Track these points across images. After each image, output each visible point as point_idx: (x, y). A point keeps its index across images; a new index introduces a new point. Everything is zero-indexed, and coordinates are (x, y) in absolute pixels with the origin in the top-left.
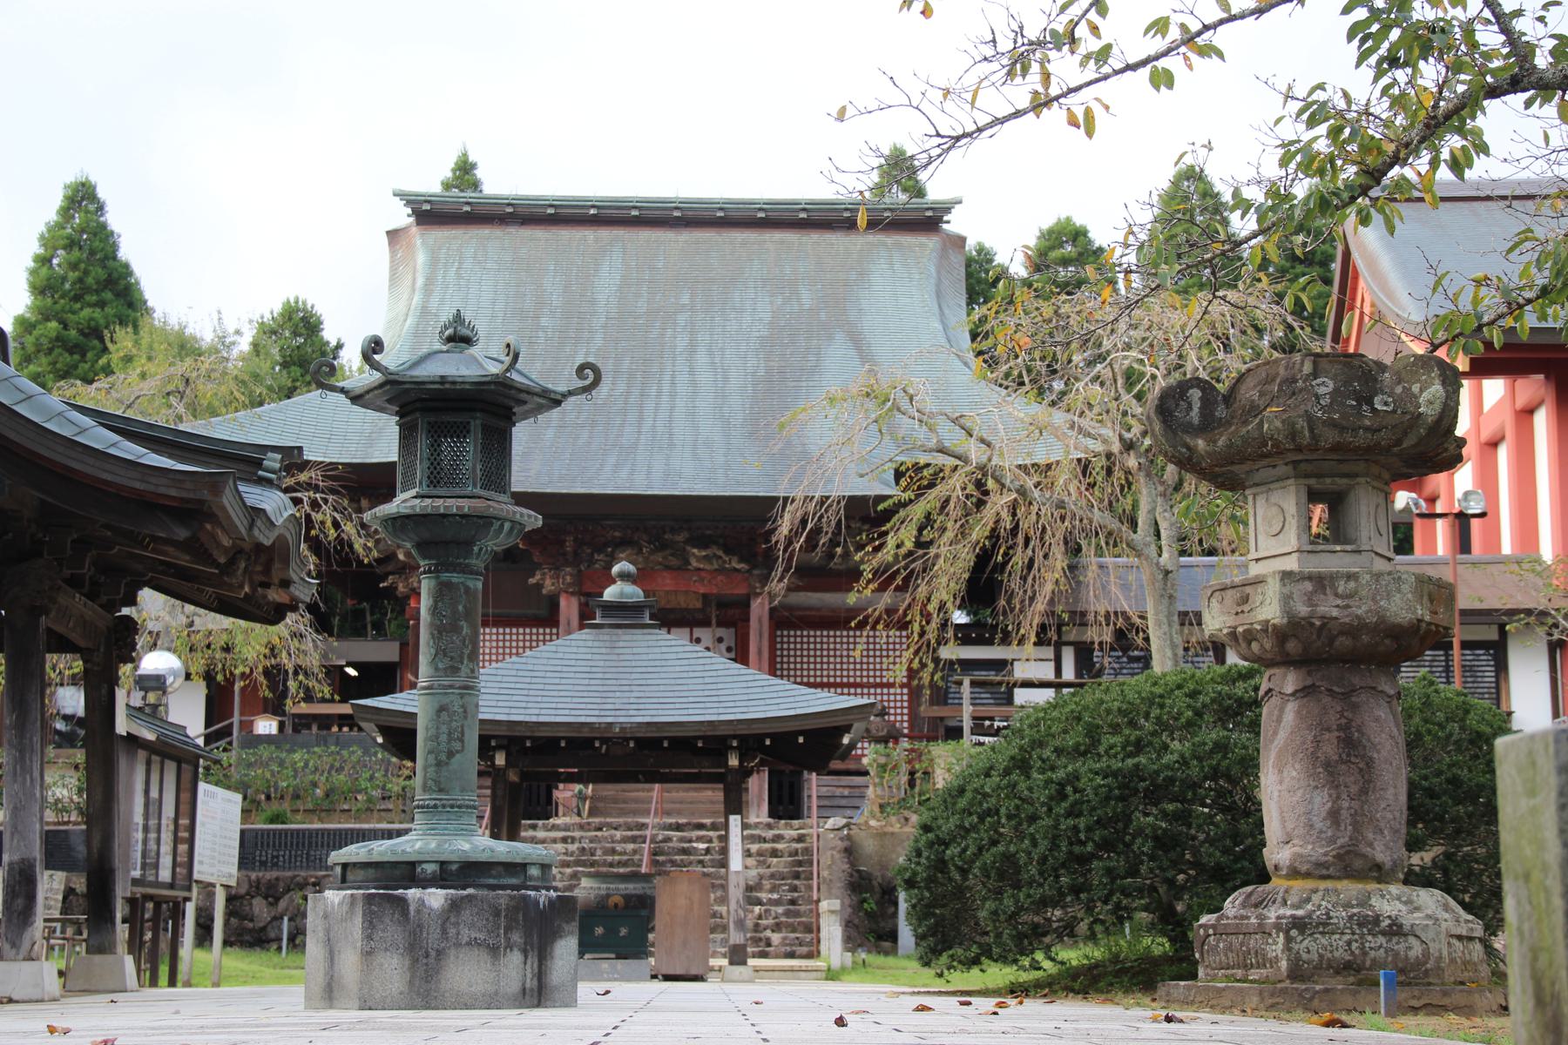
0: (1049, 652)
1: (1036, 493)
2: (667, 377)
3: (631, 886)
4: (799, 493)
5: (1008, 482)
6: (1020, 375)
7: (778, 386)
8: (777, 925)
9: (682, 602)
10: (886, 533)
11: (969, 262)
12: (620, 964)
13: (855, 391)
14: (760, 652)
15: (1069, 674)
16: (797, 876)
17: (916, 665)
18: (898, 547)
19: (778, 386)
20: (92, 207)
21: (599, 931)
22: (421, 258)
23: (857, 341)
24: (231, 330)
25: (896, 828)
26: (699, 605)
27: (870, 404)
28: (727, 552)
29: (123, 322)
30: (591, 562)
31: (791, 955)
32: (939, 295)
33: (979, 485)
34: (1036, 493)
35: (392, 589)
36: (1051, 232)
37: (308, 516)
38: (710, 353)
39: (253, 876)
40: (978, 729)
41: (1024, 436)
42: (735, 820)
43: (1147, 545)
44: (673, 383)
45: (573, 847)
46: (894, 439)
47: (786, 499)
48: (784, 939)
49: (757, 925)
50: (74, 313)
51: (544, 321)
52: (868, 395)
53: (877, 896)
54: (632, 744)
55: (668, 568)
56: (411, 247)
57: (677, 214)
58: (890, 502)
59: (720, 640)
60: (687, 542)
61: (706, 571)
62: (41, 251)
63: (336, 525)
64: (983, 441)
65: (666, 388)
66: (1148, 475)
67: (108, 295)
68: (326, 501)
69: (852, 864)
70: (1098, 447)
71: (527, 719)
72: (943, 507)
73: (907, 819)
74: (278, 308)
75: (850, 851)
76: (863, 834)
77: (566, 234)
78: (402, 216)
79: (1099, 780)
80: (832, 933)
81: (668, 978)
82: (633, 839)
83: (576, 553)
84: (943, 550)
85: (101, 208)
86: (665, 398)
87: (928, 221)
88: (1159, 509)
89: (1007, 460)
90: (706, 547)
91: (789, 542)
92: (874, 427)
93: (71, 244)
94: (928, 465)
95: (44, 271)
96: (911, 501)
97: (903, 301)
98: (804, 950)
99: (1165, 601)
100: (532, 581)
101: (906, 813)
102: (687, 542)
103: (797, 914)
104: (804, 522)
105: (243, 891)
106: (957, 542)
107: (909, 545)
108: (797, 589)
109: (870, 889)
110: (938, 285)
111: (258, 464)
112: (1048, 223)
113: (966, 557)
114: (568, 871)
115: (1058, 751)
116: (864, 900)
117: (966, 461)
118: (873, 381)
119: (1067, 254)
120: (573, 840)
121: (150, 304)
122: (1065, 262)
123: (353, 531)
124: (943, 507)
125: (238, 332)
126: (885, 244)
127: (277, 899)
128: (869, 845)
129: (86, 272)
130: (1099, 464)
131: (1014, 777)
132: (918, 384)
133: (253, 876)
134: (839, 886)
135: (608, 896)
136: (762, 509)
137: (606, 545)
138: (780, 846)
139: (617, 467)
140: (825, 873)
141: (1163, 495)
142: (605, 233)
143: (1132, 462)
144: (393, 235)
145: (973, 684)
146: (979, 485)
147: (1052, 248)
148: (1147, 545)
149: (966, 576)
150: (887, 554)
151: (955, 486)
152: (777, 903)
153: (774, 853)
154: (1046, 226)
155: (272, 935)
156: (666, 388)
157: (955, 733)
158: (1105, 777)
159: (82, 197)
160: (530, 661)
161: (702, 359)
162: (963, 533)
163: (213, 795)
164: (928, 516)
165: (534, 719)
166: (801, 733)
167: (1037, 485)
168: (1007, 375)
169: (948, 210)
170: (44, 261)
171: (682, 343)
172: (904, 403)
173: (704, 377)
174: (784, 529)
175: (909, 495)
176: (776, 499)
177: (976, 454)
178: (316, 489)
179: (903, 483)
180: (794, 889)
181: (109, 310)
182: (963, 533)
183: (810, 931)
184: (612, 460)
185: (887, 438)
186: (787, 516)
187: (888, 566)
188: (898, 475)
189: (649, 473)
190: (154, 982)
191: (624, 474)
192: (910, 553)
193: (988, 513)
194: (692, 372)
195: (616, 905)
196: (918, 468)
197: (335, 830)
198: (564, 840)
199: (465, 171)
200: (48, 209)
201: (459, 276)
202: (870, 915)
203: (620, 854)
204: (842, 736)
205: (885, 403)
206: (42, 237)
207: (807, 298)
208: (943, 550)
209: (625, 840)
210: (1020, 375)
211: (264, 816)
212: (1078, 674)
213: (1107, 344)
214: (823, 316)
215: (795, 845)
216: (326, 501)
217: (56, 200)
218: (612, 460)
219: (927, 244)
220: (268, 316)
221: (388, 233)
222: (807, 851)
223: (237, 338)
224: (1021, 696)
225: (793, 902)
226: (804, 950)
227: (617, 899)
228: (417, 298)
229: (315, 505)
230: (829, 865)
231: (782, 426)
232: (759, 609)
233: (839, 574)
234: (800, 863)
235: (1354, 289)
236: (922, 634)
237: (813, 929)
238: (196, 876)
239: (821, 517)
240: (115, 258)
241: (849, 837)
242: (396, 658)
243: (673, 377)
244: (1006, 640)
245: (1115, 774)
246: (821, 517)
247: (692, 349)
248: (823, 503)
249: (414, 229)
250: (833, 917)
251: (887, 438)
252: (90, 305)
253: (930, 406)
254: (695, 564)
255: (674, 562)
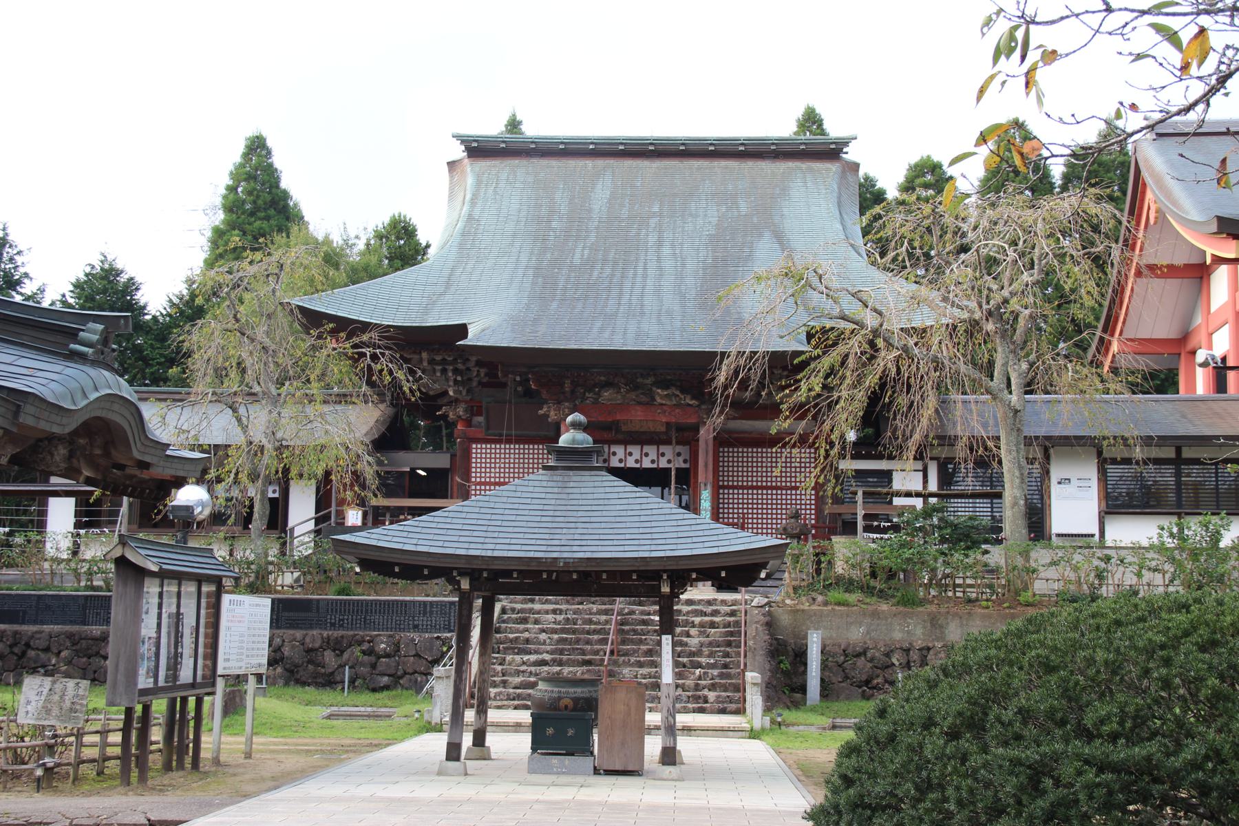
0: (919, 465)
1: (916, 351)
2: (641, 264)
3: (579, 690)
4: (733, 350)
5: (896, 344)
6: (903, 261)
7: (723, 269)
8: (713, 685)
9: (651, 427)
10: (800, 380)
11: (861, 185)
12: (567, 760)
13: (777, 272)
14: (706, 465)
15: (933, 486)
16: (729, 644)
17: (821, 480)
18: (810, 390)
19: (723, 269)
20: (264, 153)
21: (550, 731)
22: (470, 180)
23: (780, 238)
24: (353, 236)
25: (806, 606)
26: (663, 429)
27: (787, 282)
28: (682, 392)
29: (280, 230)
30: (584, 399)
31: (723, 711)
32: (839, 205)
33: (872, 344)
34: (916, 351)
35: (445, 417)
36: (916, 166)
37: (369, 366)
38: (673, 246)
39: (325, 634)
40: (868, 529)
41: (904, 305)
42: (667, 640)
43: (1001, 390)
44: (645, 269)
45: (560, 618)
46: (807, 309)
47: (723, 354)
48: (718, 697)
49: (697, 685)
50: (250, 224)
51: (554, 224)
52: (787, 274)
53: (791, 658)
54: (575, 577)
55: (640, 403)
56: (463, 172)
57: (651, 148)
58: (803, 357)
59: (679, 454)
60: (654, 384)
61: (667, 406)
62: (231, 183)
63: (391, 373)
64: (875, 310)
65: (640, 271)
66: (1003, 337)
67: (272, 212)
68: (383, 355)
69: (772, 635)
70: (966, 315)
71: (484, 553)
72: (843, 363)
73: (814, 599)
74: (387, 221)
75: (771, 625)
76: (780, 610)
77: (572, 163)
78: (458, 151)
79: (1090, 775)
80: (755, 700)
81: (609, 773)
82: (606, 612)
83: (573, 392)
84: (844, 394)
85: (269, 153)
86: (639, 279)
87: (831, 152)
88: (1011, 363)
89: (894, 324)
90: (667, 388)
91: (726, 387)
92: (791, 300)
93: (250, 177)
94: (832, 328)
95: (231, 196)
96: (819, 357)
97: (814, 215)
98: (733, 706)
99: (1015, 433)
100: (541, 412)
101: (814, 594)
102: (654, 384)
103: (728, 676)
104: (736, 373)
105: (317, 645)
106: (855, 387)
107: (818, 389)
108: (734, 418)
109: (785, 653)
110: (839, 197)
111: (73, 335)
112: (914, 159)
113: (861, 395)
114: (556, 636)
115: (1025, 714)
116: (781, 662)
117: (862, 325)
118: (790, 264)
119: (928, 177)
120: (561, 612)
121: (306, 219)
122: (926, 186)
123: (403, 377)
124: (843, 363)
125: (357, 237)
126: (801, 169)
127: (342, 652)
128: (785, 619)
129: (258, 197)
130: (961, 328)
131: (964, 744)
132: (825, 265)
133: (325, 634)
134: (760, 658)
135: (560, 698)
136: (704, 362)
137: (595, 386)
138: (717, 619)
139: (602, 330)
140: (750, 643)
141: (1013, 352)
142: (600, 163)
143: (990, 327)
144: (452, 165)
145: (864, 493)
146: (872, 344)
147: (917, 177)
148: (1001, 390)
149: (861, 414)
150: (802, 395)
151: (855, 345)
152: (713, 666)
153: (713, 625)
154: (913, 162)
155: (338, 679)
156: (640, 271)
157: (849, 528)
158: (1101, 770)
159: (257, 147)
160: (493, 499)
161: (666, 251)
162: (859, 381)
163: (240, 603)
164: (832, 368)
165: (489, 554)
166: (723, 568)
167: (916, 344)
168: (894, 260)
169: (846, 144)
170: (232, 189)
171: (652, 239)
172: (815, 281)
173: (668, 264)
174: (722, 378)
175: (819, 351)
176: (715, 353)
177: (871, 321)
178: (374, 346)
179: (813, 342)
180: (727, 655)
181: (273, 222)
182: (859, 381)
183: (739, 691)
184: (598, 324)
185: (801, 308)
186: (724, 368)
187: (802, 405)
188: (810, 336)
189: (625, 334)
190: (181, 766)
191: (607, 334)
192: (819, 395)
193: (880, 364)
194: (659, 260)
195: (566, 707)
196: (824, 331)
197: (385, 601)
198: (554, 612)
199: (514, 125)
200: (234, 154)
201: (495, 192)
202: (786, 673)
203: (596, 623)
204: (760, 572)
205: (799, 280)
206: (231, 173)
207: (744, 207)
208: (844, 394)
209: (600, 612)
210: (903, 261)
211: (334, 588)
212: (940, 486)
213: (971, 236)
214: (755, 220)
215: (728, 619)
216: (383, 355)
217: (239, 148)
218: (598, 324)
219: (833, 167)
220: (381, 226)
221: (448, 163)
222: (737, 624)
223: (357, 241)
224: (897, 501)
225: (726, 666)
226: (733, 706)
227: (567, 701)
228: (466, 208)
229: (374, 357)
230: (755, 636)
231: (720, 298)
232: (706, 434)
233: (764, 407)
234: (731, 634)
235: (1142, 200)
236: (827, 456)
237: (740, 688)
238: (220, 671)
239: (750, 369)
240: (278, 187)
241: (769, 613)
242: (448, 466)
243: (645, 264)
244: (891, 457)
245: (1115, 768)
246: (750, 369)
247: (660, 243)
248: (751, 358)
249: (466, 161)
250: (756, 689)
251: (801, 308)
252: (260, 219)
253: (835, 284)
254: (659, 400)
255: (644, 399)
